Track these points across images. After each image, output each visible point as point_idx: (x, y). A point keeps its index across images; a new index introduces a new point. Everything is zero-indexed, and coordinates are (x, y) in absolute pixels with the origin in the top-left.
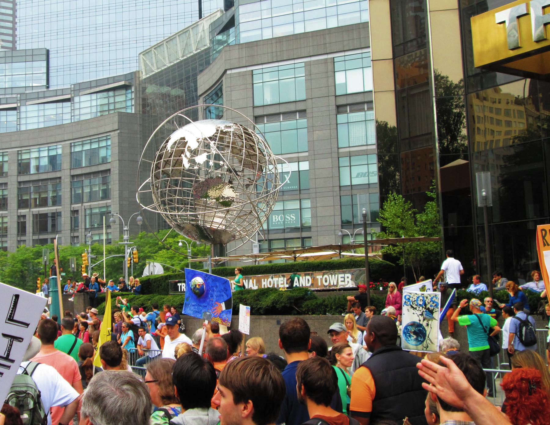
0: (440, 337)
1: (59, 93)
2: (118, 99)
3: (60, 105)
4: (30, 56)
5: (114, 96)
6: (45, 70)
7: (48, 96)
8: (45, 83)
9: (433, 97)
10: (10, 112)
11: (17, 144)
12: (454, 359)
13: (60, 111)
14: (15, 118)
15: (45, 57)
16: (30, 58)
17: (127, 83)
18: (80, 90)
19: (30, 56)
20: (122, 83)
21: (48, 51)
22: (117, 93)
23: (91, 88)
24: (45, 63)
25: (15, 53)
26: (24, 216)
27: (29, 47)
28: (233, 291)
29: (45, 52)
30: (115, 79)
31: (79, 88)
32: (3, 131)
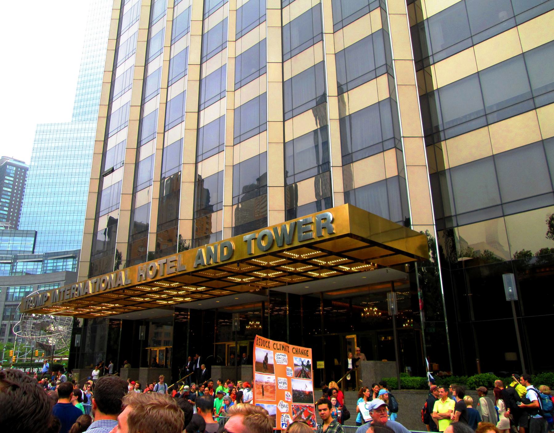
0: (244, 393)
1: (37, 257)
2: (59, 264)
3: (36, 263)
4: (26, 234)
5: (57, 262)
6: (33, 242)
7: (31, 257)
8: (31, 249)
9: (267, 273)
10: (6, 265)
11: (8, 283)
12: (463, 264)
13: (36, 267)
14: (9, 268)
15: (34, 235)
16: (25, 235)
17: (74, 255)
18: (48, 256)
19: (26, 234)
20: (71, 255)
21: (36, 232)
22: (59, 261)
23: (24, 259)
24: (33, 239)
25: (17, 232)
26: (5, 325)
27: (26, 229)
28: (233, 329)
29: (34, 233)
30: (67, 252)
31: (48, 256)
32: (2, 275)
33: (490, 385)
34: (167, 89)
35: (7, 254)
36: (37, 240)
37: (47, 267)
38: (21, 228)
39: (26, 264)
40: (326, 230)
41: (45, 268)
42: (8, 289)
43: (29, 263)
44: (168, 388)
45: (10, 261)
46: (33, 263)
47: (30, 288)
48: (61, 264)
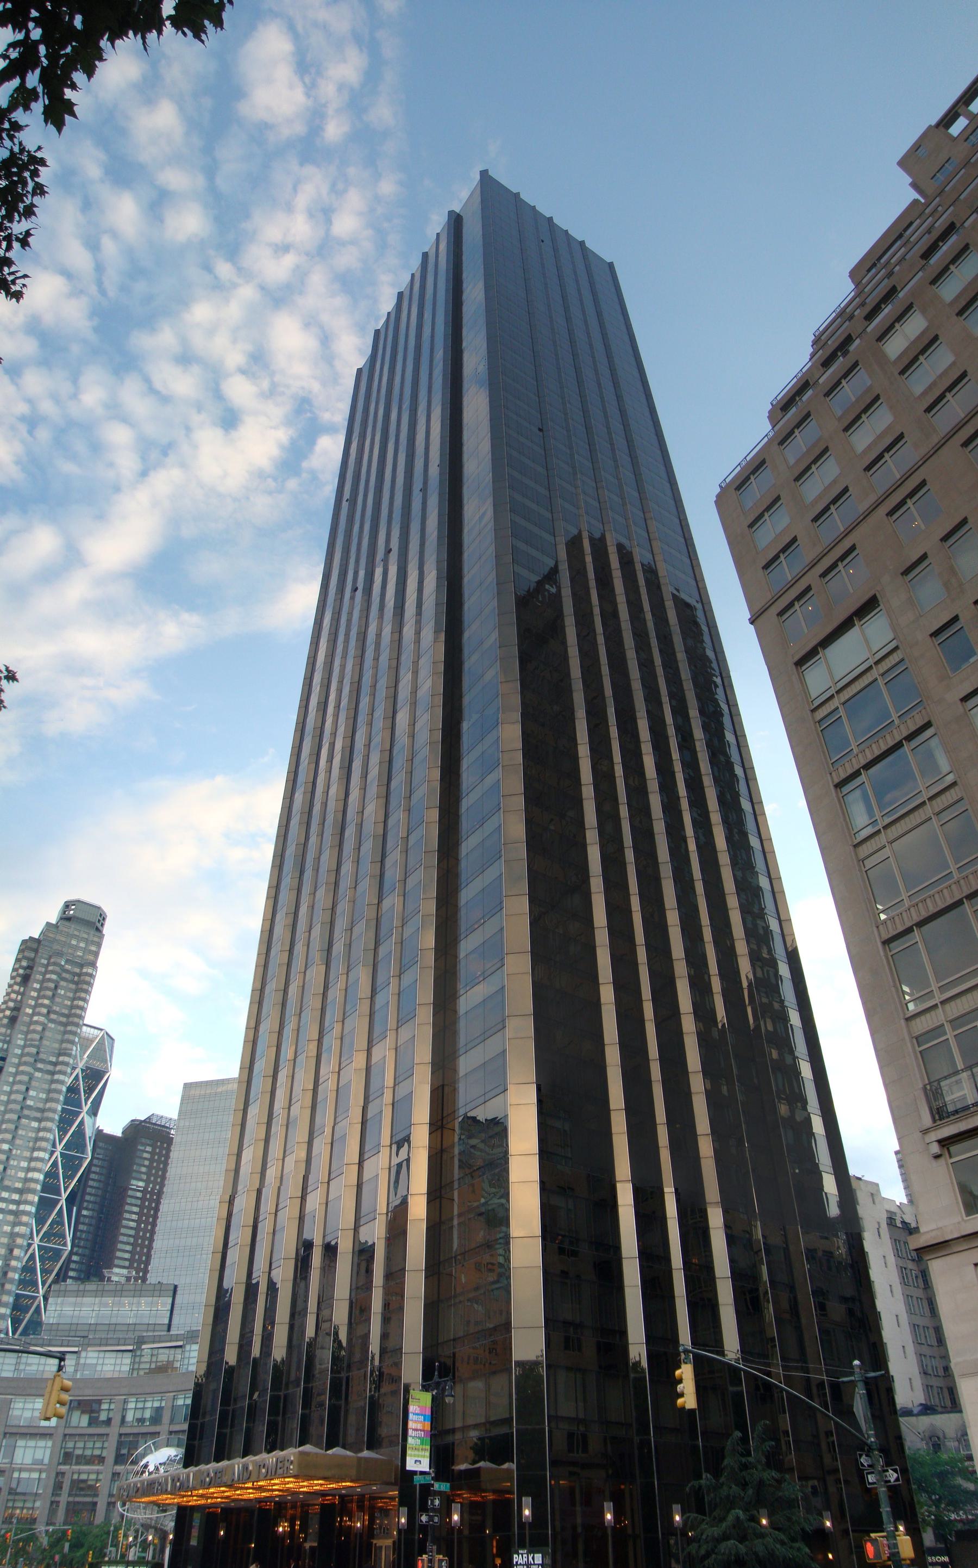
1: (122, 1342)
4: (159, 1290)
6: (169, 1307)
8: (166, 1321)
19: (159, 1290)
21: (176, 1287)
23: (100, 1345)
24: (170, 1300)
29: (172, 1288)
33: (964, 1524)
34: (339, 1073)
35: (147, 1331)
36: (177, 1301)
37: (140, 1363)
38: (152, 1278)
39: (102, 1355)
40: (196, 369)
41: (136, 1366)
42: (125, 1402)
43: (108, 1355)
44: (936, 644)
45: (131, 1348)
46: (114, 1354)
47: (161, 1400)
48: (112, 1361)
